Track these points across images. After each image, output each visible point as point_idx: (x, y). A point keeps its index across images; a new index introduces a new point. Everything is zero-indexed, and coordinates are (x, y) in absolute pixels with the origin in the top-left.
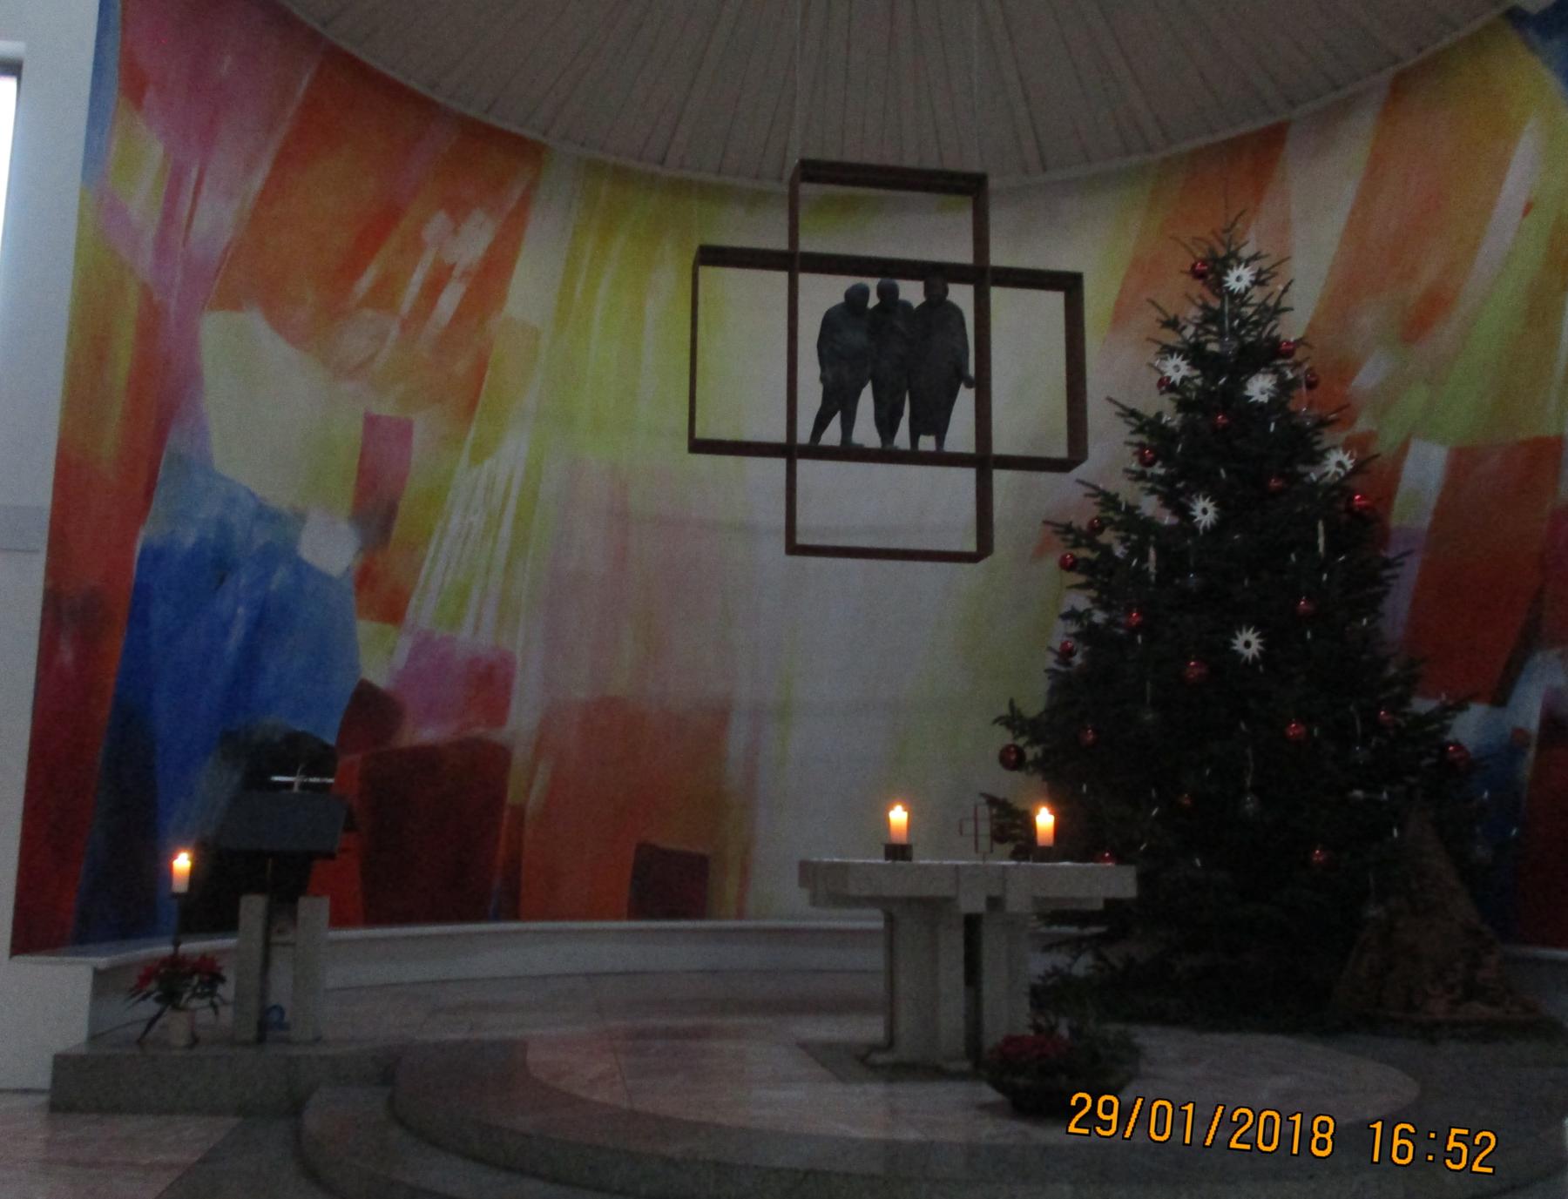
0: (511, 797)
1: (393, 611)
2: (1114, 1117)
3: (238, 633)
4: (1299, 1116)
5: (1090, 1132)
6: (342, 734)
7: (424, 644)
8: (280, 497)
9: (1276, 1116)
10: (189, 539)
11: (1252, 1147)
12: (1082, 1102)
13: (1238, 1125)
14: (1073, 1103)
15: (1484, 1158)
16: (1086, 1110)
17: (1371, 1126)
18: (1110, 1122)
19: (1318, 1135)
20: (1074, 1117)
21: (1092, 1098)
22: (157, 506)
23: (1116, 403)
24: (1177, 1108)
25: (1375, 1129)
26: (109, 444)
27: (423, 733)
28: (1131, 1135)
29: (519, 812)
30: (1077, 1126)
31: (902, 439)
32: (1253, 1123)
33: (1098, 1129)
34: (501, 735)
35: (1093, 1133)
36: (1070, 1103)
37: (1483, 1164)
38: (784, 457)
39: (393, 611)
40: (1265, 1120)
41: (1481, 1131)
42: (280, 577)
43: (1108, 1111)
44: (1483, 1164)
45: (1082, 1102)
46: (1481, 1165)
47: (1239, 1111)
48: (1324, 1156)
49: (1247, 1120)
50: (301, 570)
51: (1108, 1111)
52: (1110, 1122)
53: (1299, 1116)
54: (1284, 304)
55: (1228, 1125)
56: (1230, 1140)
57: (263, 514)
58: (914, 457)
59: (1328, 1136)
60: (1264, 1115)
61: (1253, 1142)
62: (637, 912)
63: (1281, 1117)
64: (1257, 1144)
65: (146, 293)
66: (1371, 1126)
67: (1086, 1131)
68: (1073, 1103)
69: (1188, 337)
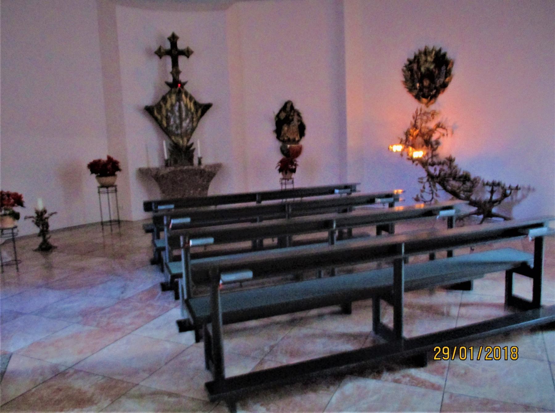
2: (448, 353)
4: (472, 347)
5: (441, 359)
12: (437, 350)
13: (487, 352)
14: (435, 350)
24: (468, 349)
28: (480, 359)
32: (492, 351)
33: (443, 358)
35: (442, 359)
36: (434, 350)
37: (489, 357)
38: (249, 240)
40: (462, 350)
41: (436, 347)
44: (489, 357)
45: (437, 350)
46: (437, 357)
49: (439, 350)
53: (472, 347)
54: (103, 375)
56: (434, 357)
59: (516, 353)
60: (461, 348)
61: (493, 357)
63: (466, 348)
68: (435, 350)
69: (287, 135)
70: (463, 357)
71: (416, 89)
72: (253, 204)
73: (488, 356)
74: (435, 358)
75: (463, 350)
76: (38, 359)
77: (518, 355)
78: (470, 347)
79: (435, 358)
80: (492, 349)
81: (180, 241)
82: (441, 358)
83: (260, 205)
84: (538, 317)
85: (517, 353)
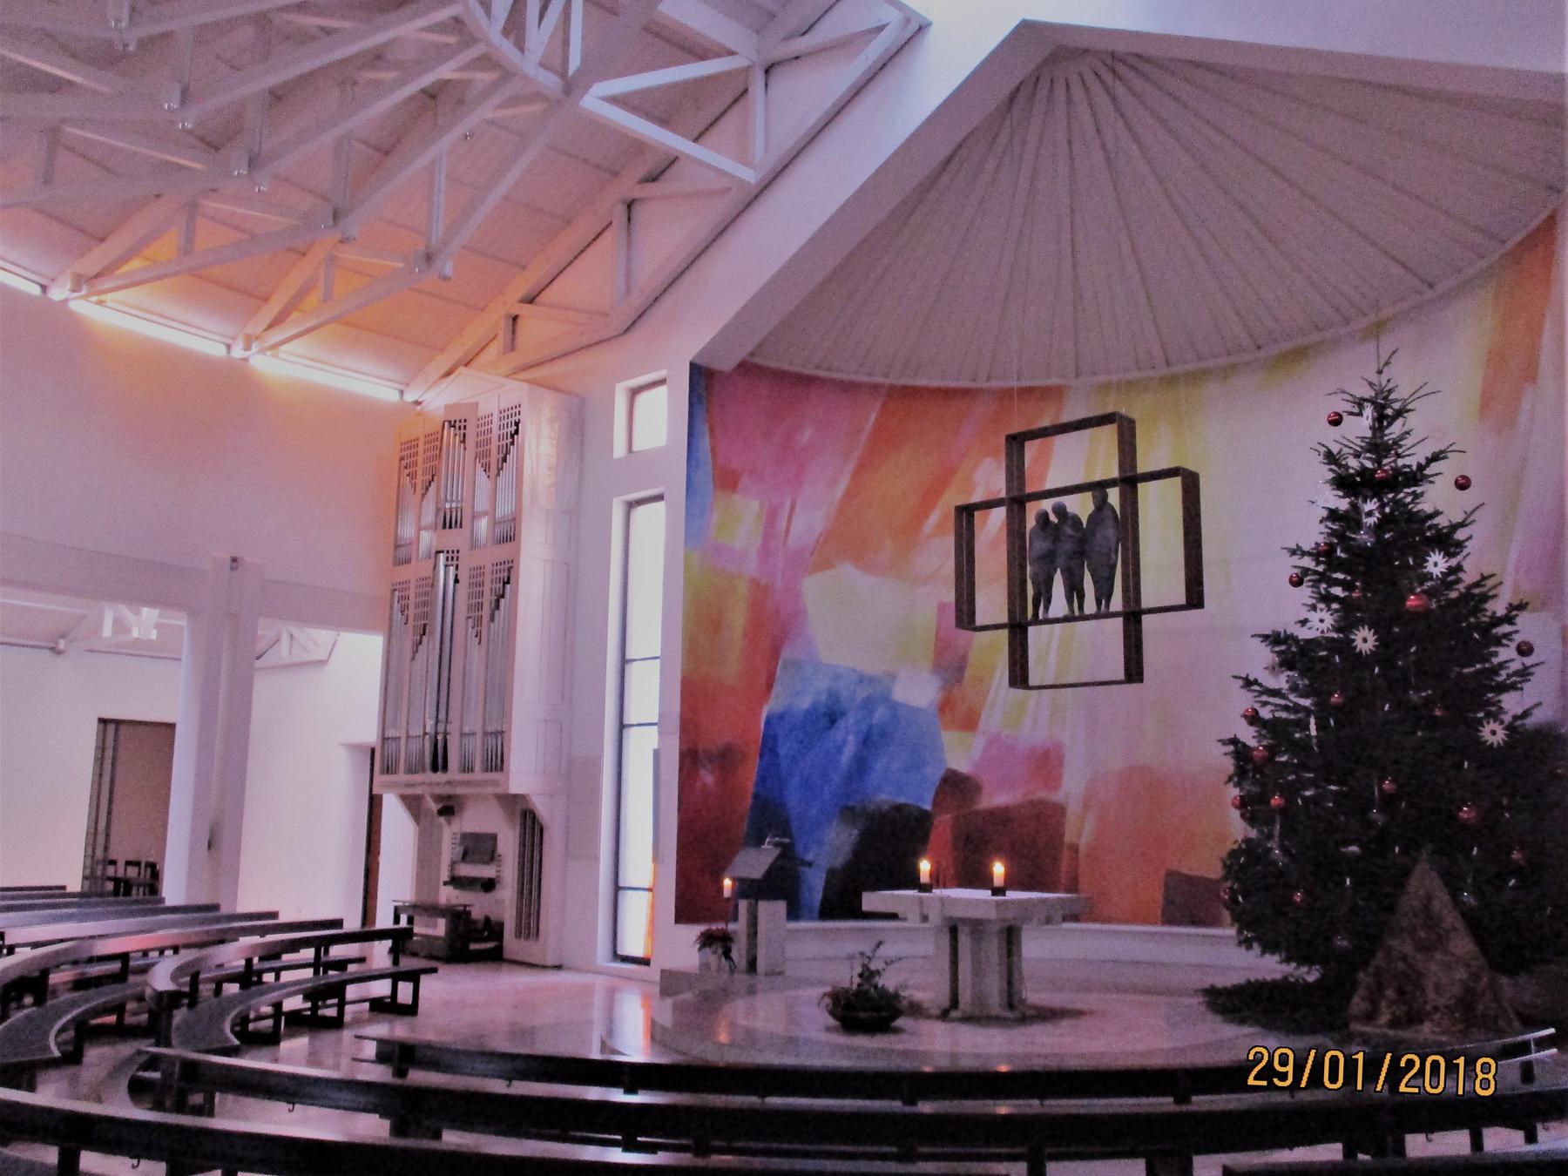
0: (1068, 838)
1: (969, 722)
2: (1290, 1069)
3: (849, 751)
6: (935, 804)
7: (994, 741)
8: (872, 666)
9: (1441, 1060)
10: (805, 703)
11: (1420, 1090)
12: (1410, 1063)
14: (1403, 1064)
15: (1410, 1079)
16: (1415, 1070)
17: (1454, 1062)
18: (1286, 1074)
19: (1481, 1076)
20: (1404, 1077)
21: (1420, 1059)
22: (777, 689)
23: (1285, 549)
25: (1357, 1060)
26: (731, 667)
27: (994, 798)
29: (1075, 848)
30: (1256, 1078)
31: (1090, 606)
34: (1057, 797)
36: (1399, 1064)
37: (1409, 1084)
39: (969, 722)
42: (880, 714)
43: (1284, 1063)
44: (1409, 1084)
45: (1410, 1063)
47: (1253, 1052)
48: (1487, 1095)
50: (894, 706)
51: (1284, 1063)
52: (1286, 1074)
53: (1462, 1059)
55: (1396, 1074)
57: (863, 679)
58: (1097, 616)
59: (1490, 1076)
62: (1169, 920)
64: (1424, 1087)
65: (754, 582)
66: (1454, 1062)
67: (1264, 1083)
68: (1403, 1064)
70: (1434, 1084)
71: (401, 1073)
72: (1164, 1104)
73: (1407, 1082)
74: (1251, 1081)
75: (1435, 1065)
76: (1069, 137)
77: (1496, 1081)
78: (1458, 1058)
79: (1251, 1081)
80: (1269, 1053)
81: (1028, 1098)
82: (1419, 1087)
83: (1184, 1108)
84: (31, 1088)
85: (1477, 1076)
